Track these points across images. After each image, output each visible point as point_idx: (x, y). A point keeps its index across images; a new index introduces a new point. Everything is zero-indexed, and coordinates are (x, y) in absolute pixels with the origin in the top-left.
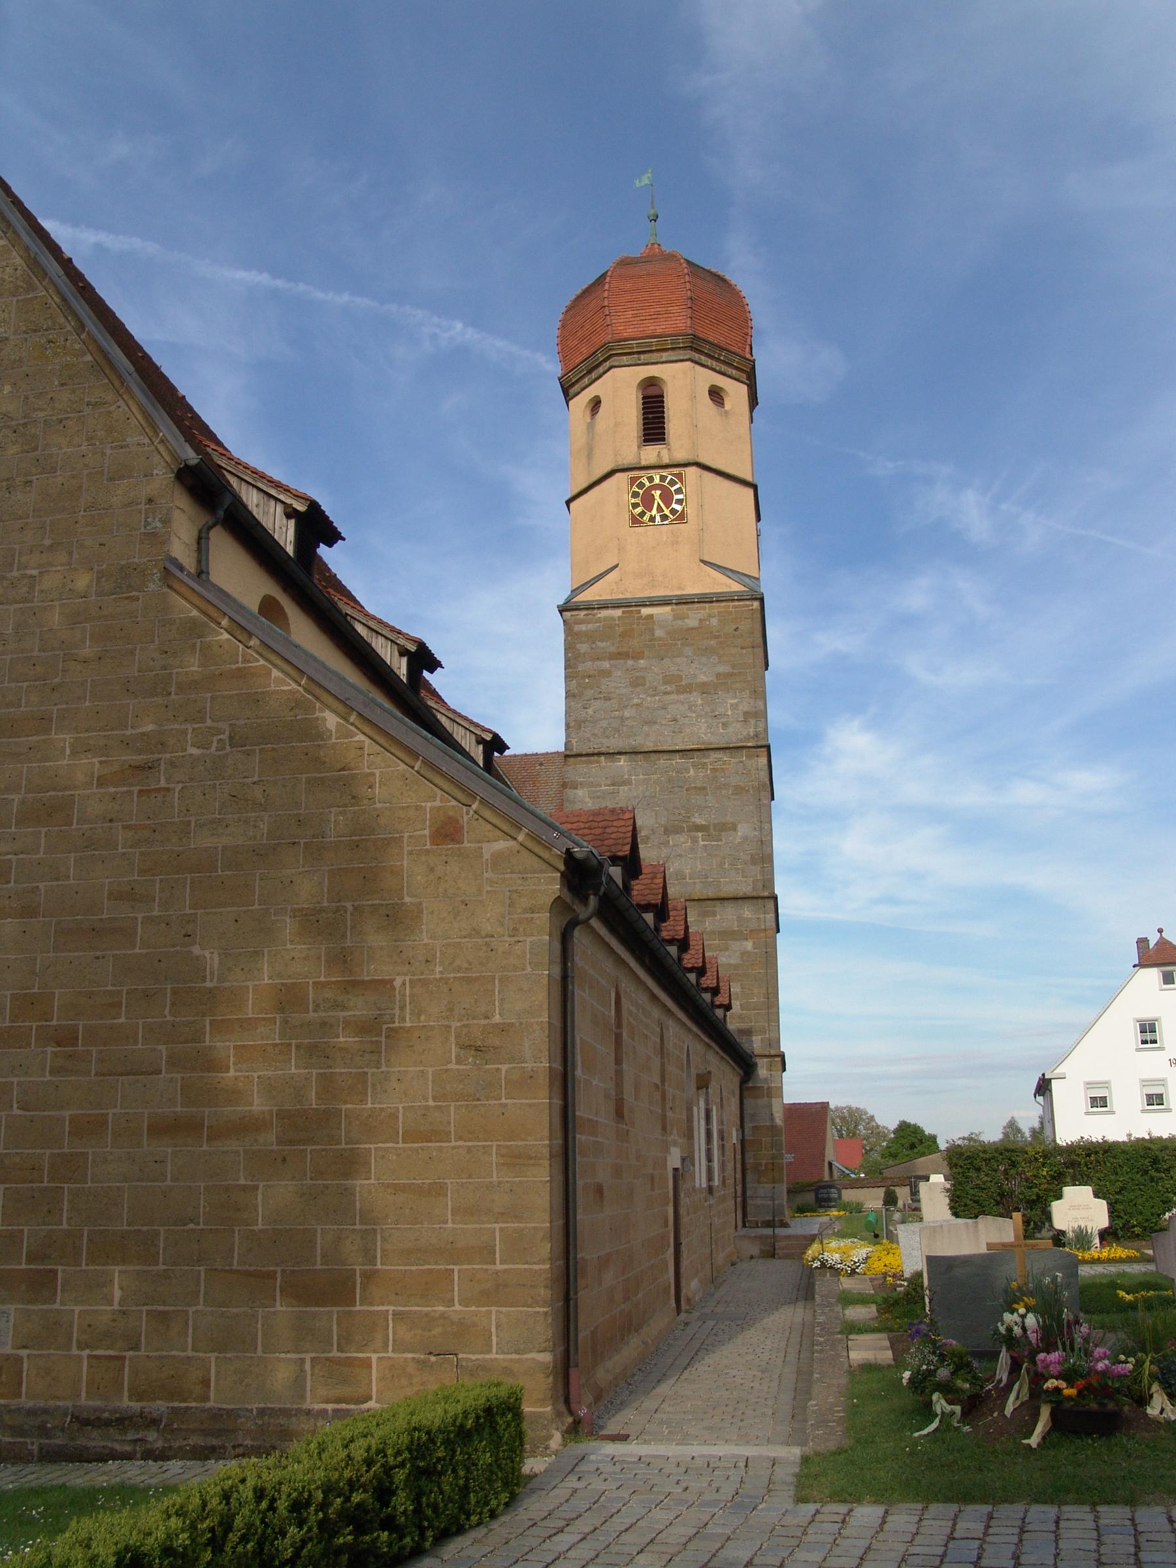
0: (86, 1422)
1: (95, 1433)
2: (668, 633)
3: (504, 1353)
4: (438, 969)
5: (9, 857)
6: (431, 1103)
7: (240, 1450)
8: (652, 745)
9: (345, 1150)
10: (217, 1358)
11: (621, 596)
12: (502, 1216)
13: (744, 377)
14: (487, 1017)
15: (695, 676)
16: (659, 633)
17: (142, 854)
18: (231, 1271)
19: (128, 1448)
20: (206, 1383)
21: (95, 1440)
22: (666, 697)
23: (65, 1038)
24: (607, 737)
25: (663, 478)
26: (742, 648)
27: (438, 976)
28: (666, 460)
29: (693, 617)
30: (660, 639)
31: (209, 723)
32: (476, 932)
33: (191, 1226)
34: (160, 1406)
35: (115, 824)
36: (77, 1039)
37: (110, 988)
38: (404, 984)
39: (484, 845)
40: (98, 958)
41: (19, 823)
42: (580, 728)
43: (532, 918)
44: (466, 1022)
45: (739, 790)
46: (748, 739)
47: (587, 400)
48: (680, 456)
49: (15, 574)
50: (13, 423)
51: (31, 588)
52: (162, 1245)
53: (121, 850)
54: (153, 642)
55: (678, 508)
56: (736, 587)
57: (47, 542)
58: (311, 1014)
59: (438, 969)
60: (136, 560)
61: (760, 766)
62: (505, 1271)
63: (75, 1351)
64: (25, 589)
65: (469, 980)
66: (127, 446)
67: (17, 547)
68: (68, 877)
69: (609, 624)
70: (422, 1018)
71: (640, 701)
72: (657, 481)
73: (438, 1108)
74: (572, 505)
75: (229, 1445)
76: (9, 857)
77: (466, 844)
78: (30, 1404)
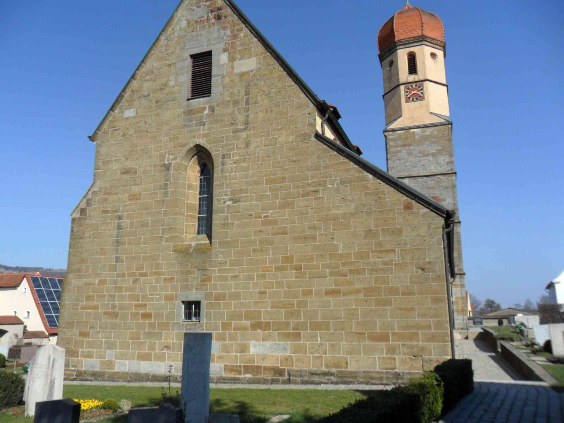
0: (313, 374)
1: (317, 377)
2: (420, 137)
3: (436, 356)
4: (408, 246)
5: (277, 218)
6: (409, 284)
7: (359, 382)
8: (415, 174)
9: (384, 298)
10: (350, 357)
11: (403, 126)
12: (432, 317)
13: (442, 48)
14: (424, 260)
15: (429, 151)
16: (417, 137)
17: (317, 216)
18: (352, 333)
19: (326, 381)
20: (347, 363)
21: (316, 379)
22: (420, 158)
23: (298, 268)
24: (401, 172)
25: (416, 86)
26: (446, 141)
27: (408, 248)
28: (417, 80)
29: (428, 131)
30: (417, 139)
31: (333, 178)
32: (419, 235)
33: (340, 320)
34: (334, 370)
35: (308, 208)
36: (302, 268)
37: (310, 254)
38: (398, 250)
39: (420, 210)
40: (306, 246)
41: (279, 208)
42: (392, 170)
43: (436, 231)
44: (418, 261)
45: (446, 188)
46: (449, 171)
47: (388, 61)
48: (421, 78)
49: (271, 137)
50: (266, 93)
51: (276, 141)
52: (331, 325)
53: (310, 215)
54: (314, 155)
55: (411, 99)
56: (443, 121)
57: (279, 127)
58: (371, 260)
59: (408, 246)
60: (307, 132)
61: (453, 179)
62: (435, 332)
63: (308, 355)
64: (274, 141)
65: (418, 249)
66: (301, 98)
67: (271, 129)
68: (295, 223)
69: (400, 137)
70: (405, 260)
71: (411, 160)
72: (414, 86)
73: (411, 286)
74: (385, 97)
75: (356, 381)
76: (277, 218)
77: (414, 210)
78: (297, 369)
